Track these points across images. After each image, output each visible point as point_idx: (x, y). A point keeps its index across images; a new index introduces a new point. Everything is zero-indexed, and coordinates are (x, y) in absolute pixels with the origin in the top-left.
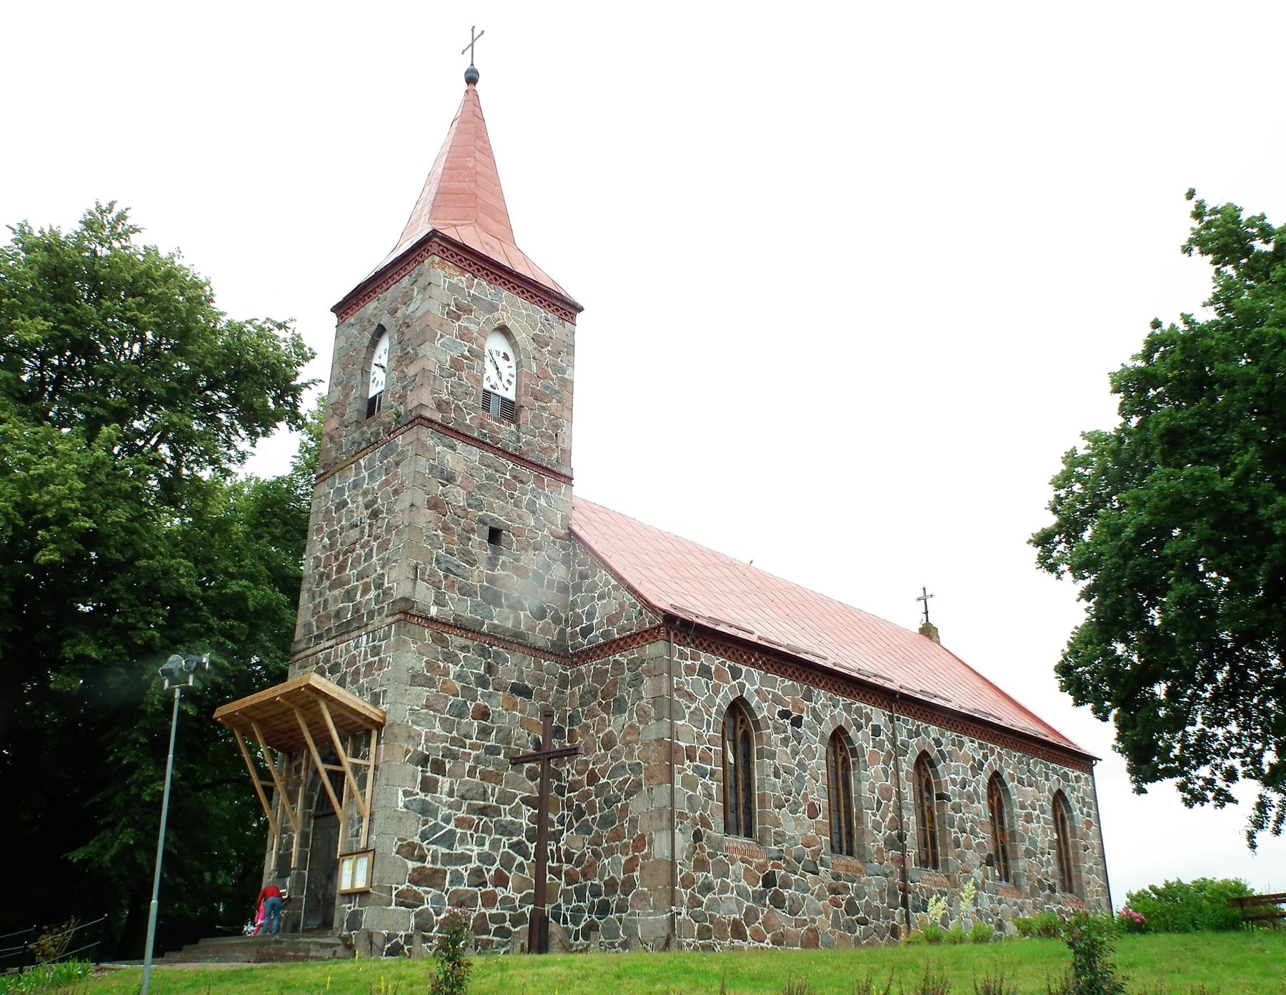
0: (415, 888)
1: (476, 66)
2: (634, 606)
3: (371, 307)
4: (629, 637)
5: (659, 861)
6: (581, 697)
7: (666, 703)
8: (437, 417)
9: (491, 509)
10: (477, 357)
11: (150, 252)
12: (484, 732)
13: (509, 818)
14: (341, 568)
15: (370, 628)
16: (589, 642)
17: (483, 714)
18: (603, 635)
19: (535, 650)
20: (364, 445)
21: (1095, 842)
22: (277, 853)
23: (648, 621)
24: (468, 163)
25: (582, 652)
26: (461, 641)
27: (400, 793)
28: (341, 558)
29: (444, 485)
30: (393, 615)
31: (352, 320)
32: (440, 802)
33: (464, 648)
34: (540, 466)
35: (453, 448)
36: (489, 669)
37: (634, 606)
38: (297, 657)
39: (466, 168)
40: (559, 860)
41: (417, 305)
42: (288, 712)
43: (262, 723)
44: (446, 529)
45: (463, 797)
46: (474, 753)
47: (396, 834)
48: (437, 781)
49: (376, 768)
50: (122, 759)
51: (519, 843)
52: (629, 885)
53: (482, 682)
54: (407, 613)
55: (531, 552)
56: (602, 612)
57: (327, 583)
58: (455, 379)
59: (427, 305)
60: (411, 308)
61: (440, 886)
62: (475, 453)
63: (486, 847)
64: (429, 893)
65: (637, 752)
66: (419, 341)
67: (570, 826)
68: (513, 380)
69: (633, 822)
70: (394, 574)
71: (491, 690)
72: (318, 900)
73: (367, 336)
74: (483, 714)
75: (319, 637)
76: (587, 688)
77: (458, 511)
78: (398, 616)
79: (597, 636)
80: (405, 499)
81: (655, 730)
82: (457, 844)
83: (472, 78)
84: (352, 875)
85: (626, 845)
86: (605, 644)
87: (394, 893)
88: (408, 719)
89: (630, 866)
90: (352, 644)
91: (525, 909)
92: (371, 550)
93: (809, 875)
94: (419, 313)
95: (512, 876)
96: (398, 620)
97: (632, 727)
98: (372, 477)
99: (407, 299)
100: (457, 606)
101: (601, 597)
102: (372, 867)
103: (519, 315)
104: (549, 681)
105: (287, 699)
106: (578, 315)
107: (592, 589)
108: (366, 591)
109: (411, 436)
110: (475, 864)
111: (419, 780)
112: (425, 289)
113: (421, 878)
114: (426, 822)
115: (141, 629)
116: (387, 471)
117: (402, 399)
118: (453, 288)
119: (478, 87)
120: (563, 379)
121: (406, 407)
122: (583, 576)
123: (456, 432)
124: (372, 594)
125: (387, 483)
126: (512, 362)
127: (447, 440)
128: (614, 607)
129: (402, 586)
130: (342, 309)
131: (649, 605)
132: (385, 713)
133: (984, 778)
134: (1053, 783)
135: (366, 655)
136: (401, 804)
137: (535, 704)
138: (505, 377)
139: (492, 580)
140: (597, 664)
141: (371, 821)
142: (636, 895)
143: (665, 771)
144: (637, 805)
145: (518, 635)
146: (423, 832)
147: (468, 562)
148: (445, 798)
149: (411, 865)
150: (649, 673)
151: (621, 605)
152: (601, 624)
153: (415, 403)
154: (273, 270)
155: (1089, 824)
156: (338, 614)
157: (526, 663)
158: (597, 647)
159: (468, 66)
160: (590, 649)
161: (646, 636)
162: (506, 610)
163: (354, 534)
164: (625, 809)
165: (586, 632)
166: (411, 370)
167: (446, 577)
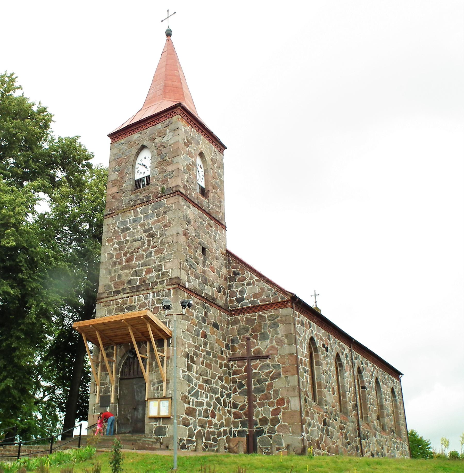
0: (187, 417)
1: (170, 28)
2: (271, 290)
3: (135, 136)
4: (268, 304)
5: (295, 411)
6: (238, 331)
7: (293, 337)
8: (184, 192)
9: (202, 238)
10: (194, 165)
11: (22, 101)
12: (206, 344)
13: (215, 386)
14: (128, 260)
15: (154, 290)
16: (242, 305)
17: (205, 336)
18: (251, 302)
19: (219, 307)
20: (139, 202)
21: (402, 411)
22: (99, 395)
23: (270, 296)
24: (169, 73)
25: (238, 309)
26: (197, 300)
27: (181, 371)
28: (128, 255)
29: (187, 225)
30: (172, 285)
31: (122, 141)
32: (193, 376)
33: (198, 304)
34: (216, 220)
35: (189, 207)
36: (206, 314)
37: (271, 290)
38: (102, 300)
39: (176, 76)
40: (231, 407)
41: (169, 137)
42: (126, 327)
43: (101, 332)
44: (189, 246)
45: (200, 375)
46: (203, 354)
47: (181, 391)
48: (192, 366)
49: (168, 358)
50: (12, 344)
51: (218, 398)
52: (275, 421)
53: (204, 321)
54: (178, 284)
55: (215, 260)
56: (250, 292)
57: (120, 267)
58: (188, 175)
59: (176, 138)
60: (165, 139)
61: (194, 416)
62: (196, 211)
63: (209, 399)
64: (191, 419)
65: (276, 359)
66: (173, 155)
67: (235, 391)
68: (204, 178)
69: (276, 392)
70: (168, 265)
71: (206, 324)
72: (128, 419)
73: (134, 151)
74: (205, 336)
75: (117, 292)
76: (242, 327)
77: (192, 238)
78: (175, 286)
79: (247, 302)
80: (173, 230)
81: (286, 349)
82: (199, 397)
83: (169, 34)
84: (155, 408)
85: (273, 403)
86: (253, 307)
87: (181, 419)
88: (182, 335)
89: (276, 412)
90: (143, 297)
91: (221, 429)
92: (151, 253)
93: (335, 421)
94: (171, 142)
95: (217, 413)
96: (176, 288)
97: (273, 347)
98: (146, 217)
99: (162, 134)
100: (194, 284)
101: (248, 284)
102: (171, 405)
103: (206, 147)
104: (224, 322)
105: (126, 322)
106: (225, 150)
107: (243, 279)
108: (149, 271)
109: (173, 200)
110: (205, 407)
111: (187, 365)
112: (174, 130)
113: (190, 412)
114: (189, 385)
115: (30, 282)
116: (158, 215)
117: (165, 181)
118: (186, 131)
119: (172, 38)
120: (220, 180)
121: (167, 185)
122: (235, 274)
123: (190, 200)
124: (154, 274)
125: (158, 221)
126: (203, 170)
127: (188, 203)
128: (257, 290)
129: (175, 271)
130: (114, 136)
131: (281, 290)
132: (171, 332)
133: (374, 380)
134: (390, 384)
135: (153, 303)
136: (181, 376)
137: (220, 332)
138: (202, 176)
139: (204, 272)
140: (249, 316)
141: (167, 383)
142: (281, 426)
143: (295, 369)
144: (278, 384)
145: (214, 299)
146: (189, 390)
147: (197, 263)
148: (195, 375)
149: (186, 406)
150: (282, 322)
151: (262, 289)
152: (249, 297)
153: (174, 184)
154: (84, 113)
155: (400, 403)
156: (129, 282)
157: (217, 312)
158: (247, 308)
159: (167, 28)
160: (242, 308)
161: (279, 305)
162: (209, 287)
163: (137, 244)
164: (270, 386)
165: (239, 301)
166: (169, 168)
167: (190, 269)
